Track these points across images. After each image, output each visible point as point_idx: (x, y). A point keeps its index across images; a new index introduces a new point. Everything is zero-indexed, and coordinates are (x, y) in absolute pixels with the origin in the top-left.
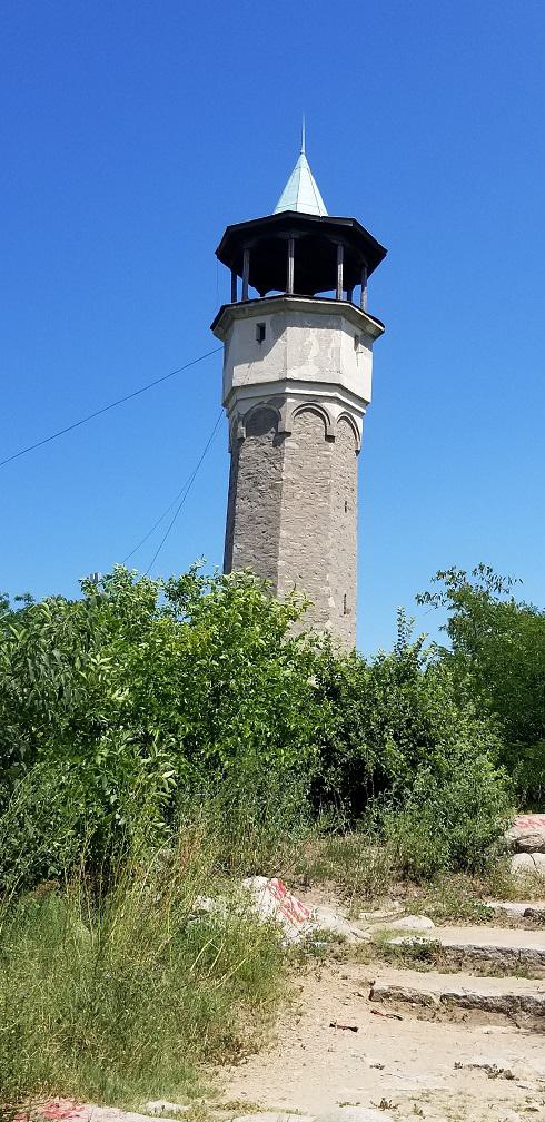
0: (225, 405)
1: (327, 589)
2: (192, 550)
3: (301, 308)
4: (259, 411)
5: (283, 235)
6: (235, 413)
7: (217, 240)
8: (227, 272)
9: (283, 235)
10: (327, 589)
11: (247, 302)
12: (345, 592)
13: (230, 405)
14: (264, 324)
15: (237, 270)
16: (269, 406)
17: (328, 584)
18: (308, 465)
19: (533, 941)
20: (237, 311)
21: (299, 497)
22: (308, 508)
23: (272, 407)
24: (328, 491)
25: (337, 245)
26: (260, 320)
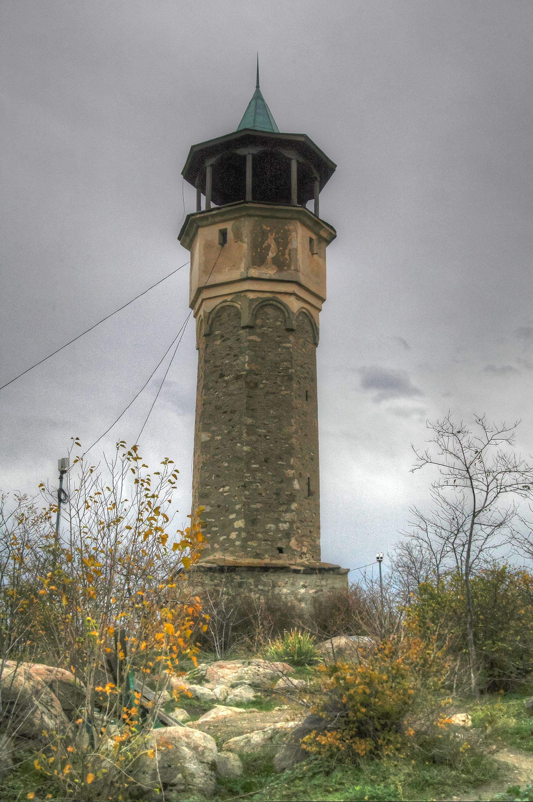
1: (290, 473)
2: (334, 664)
3: (258, 213)
4: (223, 308)
5: (242, 151)
6: (201, 313)
7: (181, 160)
9: (242, 151)
10: (290, 473)
11: (208, 211)
12: (308, 475)
13: (197, 307)
14: (226, 229)
15: (201, 189)
16: (232, 304)
17: (292, 467)
18: (271, 356)
20: (202, 219)
21: (262, 386)
22: (271, 397)
23: (235, 304)
24: (290, 378)
25: (290, 160)
26: (222, 226)
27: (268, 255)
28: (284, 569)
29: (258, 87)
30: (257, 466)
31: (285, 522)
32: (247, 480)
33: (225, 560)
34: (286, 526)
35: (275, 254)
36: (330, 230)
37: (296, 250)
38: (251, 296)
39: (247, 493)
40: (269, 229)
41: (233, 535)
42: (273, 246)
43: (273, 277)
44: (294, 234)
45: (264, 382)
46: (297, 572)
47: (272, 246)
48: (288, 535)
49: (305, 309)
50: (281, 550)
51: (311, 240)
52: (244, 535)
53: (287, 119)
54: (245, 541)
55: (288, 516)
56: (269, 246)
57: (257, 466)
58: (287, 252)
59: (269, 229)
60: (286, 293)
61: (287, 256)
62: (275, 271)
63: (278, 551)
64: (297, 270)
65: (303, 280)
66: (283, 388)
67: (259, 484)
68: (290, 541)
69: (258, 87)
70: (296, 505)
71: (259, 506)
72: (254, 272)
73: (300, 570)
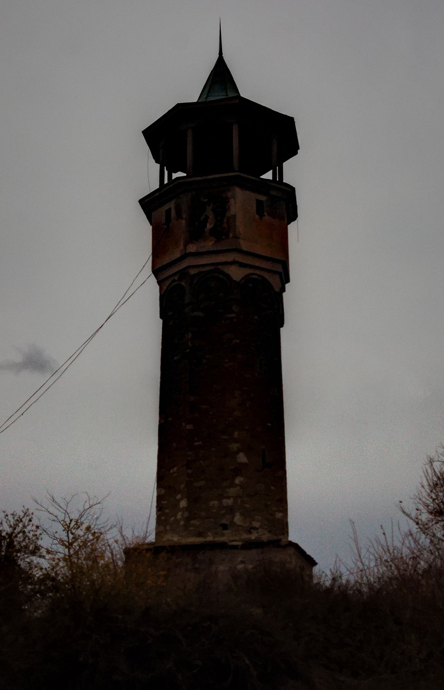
1: (235, 446)
26: (166, 207)
27: (206, 226)
28: (223, 546)
29: (221, 53)
30: (200, 443)
31: (229, 498)
32: (189, 458)
33: (172, 540)
34: (230, 502)
35: (212, 226)
36: (286, 188)
37: (235, 216)
38: (193, 272)
39: (190, 471)
40: (206, 200)
41: (179, 516)
42: (211, 216)
43: (212, 249)
44: (232, 201)
45: (207, 356)
46: (235, 547)
47: (210, 217)
48: (231, 510)
49: (256, 274)
50: (225, 527)
51: (259, 203)
52: (186, 514)
54: (188, 520)
55: (232, 491)
56: (207, 217)
57: (200, 443)
58: (225, 220)
59: (206, 200)
60: (226, 263)
61: (225, 225)
62: (213, 242)
63: (221, 528)
64: (236, 237)
65: (244, 246)
66: (227, 360)
67: (201, 462)
68: (234, 517)
69: (221, 53)
70: (242, 479)
71: (202, 483)
72: (192, 248)
73: (238, 545)
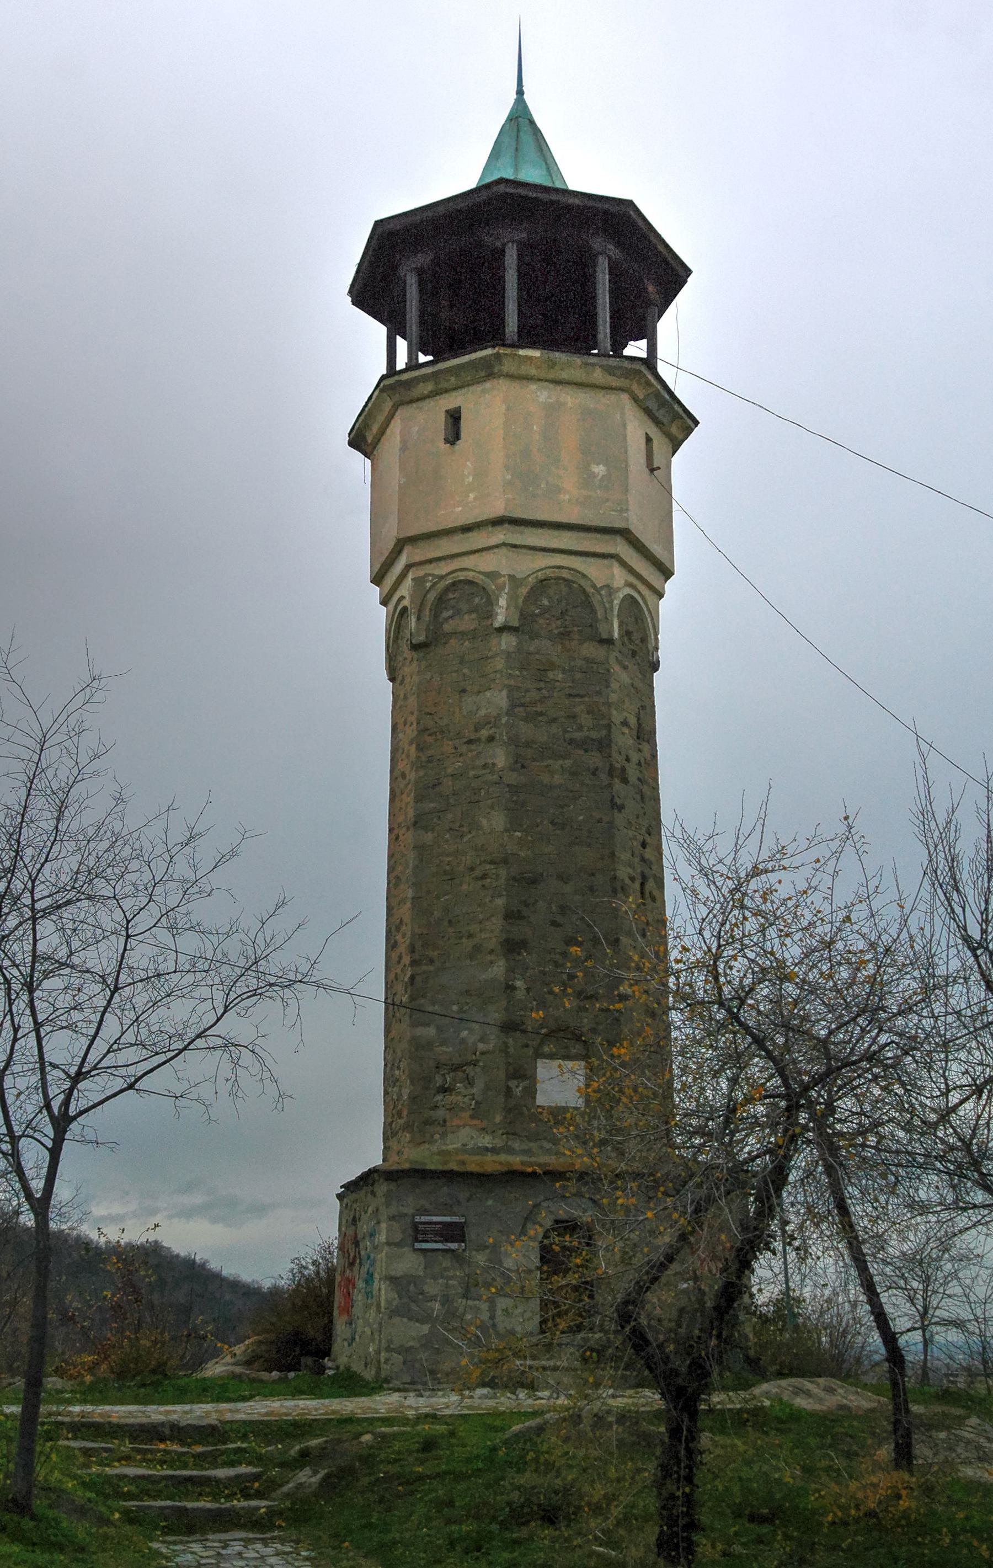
0: (377, 579)
8: (379, 331)
15: (396, 328)
19: (401, 363)
29: (520, 92)
51: (649, 440)
53: (586, 168)
69: (520, 92)
